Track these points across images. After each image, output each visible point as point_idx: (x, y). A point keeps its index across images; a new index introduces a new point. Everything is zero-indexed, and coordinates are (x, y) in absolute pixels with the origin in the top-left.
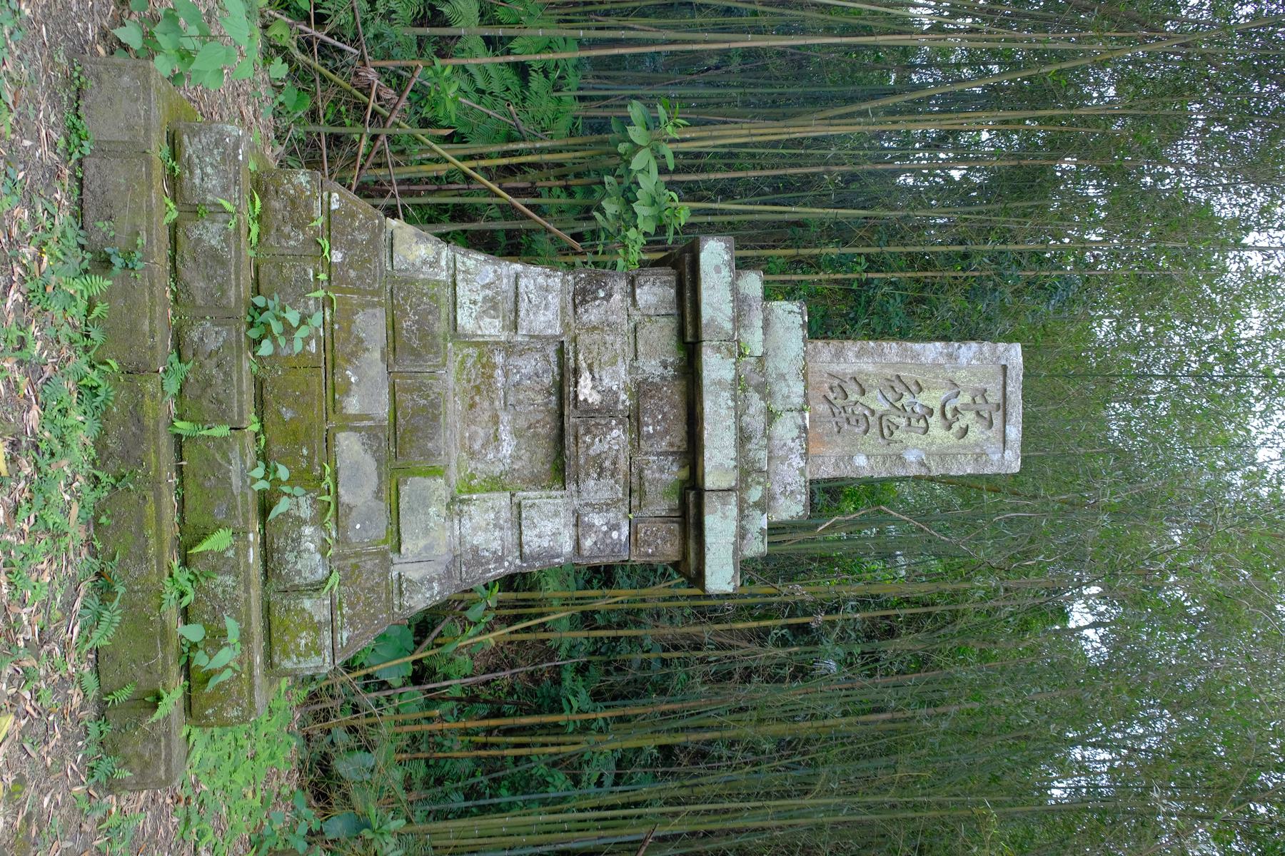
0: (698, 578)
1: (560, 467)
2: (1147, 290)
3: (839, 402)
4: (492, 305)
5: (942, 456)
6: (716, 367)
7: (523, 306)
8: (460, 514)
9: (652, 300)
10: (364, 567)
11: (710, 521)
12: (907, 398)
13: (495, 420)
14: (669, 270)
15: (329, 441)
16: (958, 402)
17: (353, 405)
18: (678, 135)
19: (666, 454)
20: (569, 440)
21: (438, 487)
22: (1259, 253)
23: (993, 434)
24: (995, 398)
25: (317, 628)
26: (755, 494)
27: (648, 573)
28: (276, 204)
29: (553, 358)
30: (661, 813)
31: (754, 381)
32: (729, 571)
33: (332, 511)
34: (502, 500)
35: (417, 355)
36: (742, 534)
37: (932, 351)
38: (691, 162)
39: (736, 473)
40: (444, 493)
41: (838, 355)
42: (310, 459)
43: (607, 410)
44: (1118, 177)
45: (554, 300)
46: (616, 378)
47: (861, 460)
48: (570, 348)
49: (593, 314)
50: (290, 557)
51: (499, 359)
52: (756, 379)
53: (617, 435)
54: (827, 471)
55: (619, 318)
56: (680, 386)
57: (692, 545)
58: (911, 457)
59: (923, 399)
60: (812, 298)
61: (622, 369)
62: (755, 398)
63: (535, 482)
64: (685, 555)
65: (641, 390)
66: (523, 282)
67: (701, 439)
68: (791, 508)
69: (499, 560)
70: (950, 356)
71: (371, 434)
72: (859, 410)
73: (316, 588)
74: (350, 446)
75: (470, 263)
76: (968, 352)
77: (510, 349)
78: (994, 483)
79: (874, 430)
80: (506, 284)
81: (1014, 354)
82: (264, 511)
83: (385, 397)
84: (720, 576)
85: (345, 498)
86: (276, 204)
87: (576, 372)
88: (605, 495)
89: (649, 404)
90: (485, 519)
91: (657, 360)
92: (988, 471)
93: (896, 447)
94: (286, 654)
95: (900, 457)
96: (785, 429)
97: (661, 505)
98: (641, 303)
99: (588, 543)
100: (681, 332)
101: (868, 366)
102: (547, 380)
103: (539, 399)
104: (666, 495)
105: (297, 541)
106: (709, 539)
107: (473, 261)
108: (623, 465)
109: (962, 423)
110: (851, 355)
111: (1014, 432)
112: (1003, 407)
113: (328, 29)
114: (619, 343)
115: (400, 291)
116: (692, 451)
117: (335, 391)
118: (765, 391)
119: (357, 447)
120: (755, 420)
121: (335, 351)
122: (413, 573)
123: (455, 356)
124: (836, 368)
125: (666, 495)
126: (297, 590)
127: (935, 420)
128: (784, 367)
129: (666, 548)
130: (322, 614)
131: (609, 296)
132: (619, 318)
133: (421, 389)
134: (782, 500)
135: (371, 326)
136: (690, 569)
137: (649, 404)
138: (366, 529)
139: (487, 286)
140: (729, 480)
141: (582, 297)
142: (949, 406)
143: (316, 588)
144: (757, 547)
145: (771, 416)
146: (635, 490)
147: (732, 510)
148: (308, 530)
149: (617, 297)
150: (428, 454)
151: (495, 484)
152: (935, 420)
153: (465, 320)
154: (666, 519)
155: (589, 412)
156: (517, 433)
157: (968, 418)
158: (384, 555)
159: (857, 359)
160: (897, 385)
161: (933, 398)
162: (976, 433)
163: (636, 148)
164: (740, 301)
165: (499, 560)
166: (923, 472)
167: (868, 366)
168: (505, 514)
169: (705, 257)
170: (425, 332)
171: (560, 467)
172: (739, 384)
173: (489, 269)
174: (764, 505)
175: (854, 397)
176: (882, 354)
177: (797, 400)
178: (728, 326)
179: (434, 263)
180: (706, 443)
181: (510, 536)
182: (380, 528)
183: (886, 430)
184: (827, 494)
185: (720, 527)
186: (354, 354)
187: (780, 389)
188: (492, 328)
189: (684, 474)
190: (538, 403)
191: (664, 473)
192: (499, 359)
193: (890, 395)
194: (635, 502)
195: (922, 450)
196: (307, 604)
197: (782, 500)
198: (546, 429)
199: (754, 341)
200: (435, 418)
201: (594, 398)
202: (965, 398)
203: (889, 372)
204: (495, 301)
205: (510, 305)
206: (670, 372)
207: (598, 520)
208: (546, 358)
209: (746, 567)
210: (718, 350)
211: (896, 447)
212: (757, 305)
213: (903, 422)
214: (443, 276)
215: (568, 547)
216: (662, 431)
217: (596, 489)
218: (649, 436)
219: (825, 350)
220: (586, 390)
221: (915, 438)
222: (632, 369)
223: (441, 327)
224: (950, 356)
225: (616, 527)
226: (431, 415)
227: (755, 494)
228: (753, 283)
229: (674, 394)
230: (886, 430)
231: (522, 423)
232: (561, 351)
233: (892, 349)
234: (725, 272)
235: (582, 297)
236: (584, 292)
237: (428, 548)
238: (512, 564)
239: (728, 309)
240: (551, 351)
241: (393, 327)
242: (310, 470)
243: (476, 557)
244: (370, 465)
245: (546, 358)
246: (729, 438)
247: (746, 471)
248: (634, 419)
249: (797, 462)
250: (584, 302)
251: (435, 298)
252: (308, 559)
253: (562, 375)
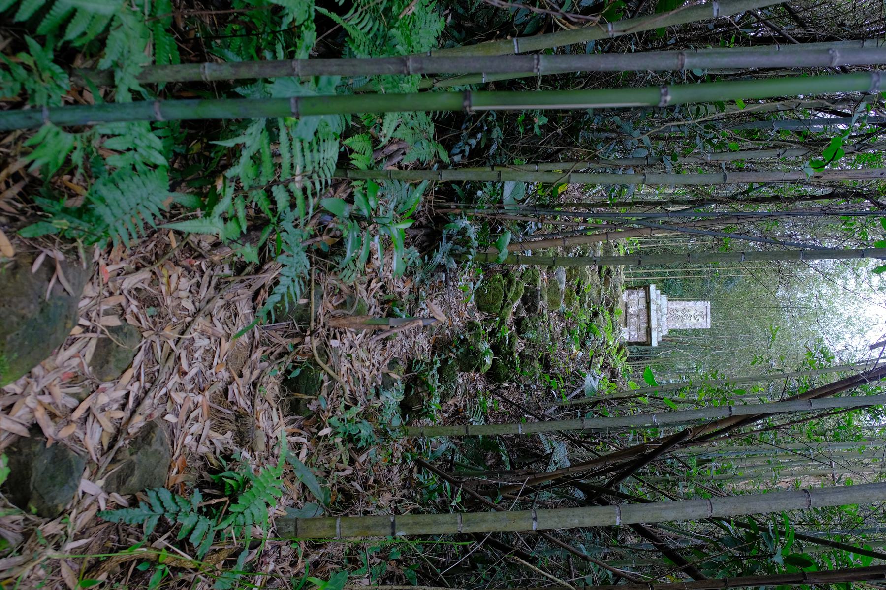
0: (650, 344)
6: (653, 307)
27: (643, 344)
30: (407, 587)
31: (659, 310)
37: (691, 303)
43: (634, 314)
46: (635, 309)
49: (632, 298)
54: (671, 328)
65: (640, 311)
68: (666, 333)
76: (699, 303)
81: (708, 304)
84: (654, 343)
91: (643, 306)
96: (664, 318)
97: (643, 331)
101: (678, 306)
112: (707, 315)
114: (636, 303)
129: (643, 339)
146: (639, 328)
157: (699, 317)
159: (676, 305)
160: (684, 310)
161: (692, 313)
162: (701, 320)
164: (657, 295)
167: (678, 306)
183: (682, 320)
184: (672, 331)
185: (654, 334)
191: (644, 326)
195: (690, 324)
199: (659, 302)
209: (659, 342)
216: (643, 318)
217: (632, 328)
220: (630, 311)
221: (688, 321)
228: (659, 292)
229: (645, 311)
230: (682, 320)
247: (659, 325)
248: (639, 316)
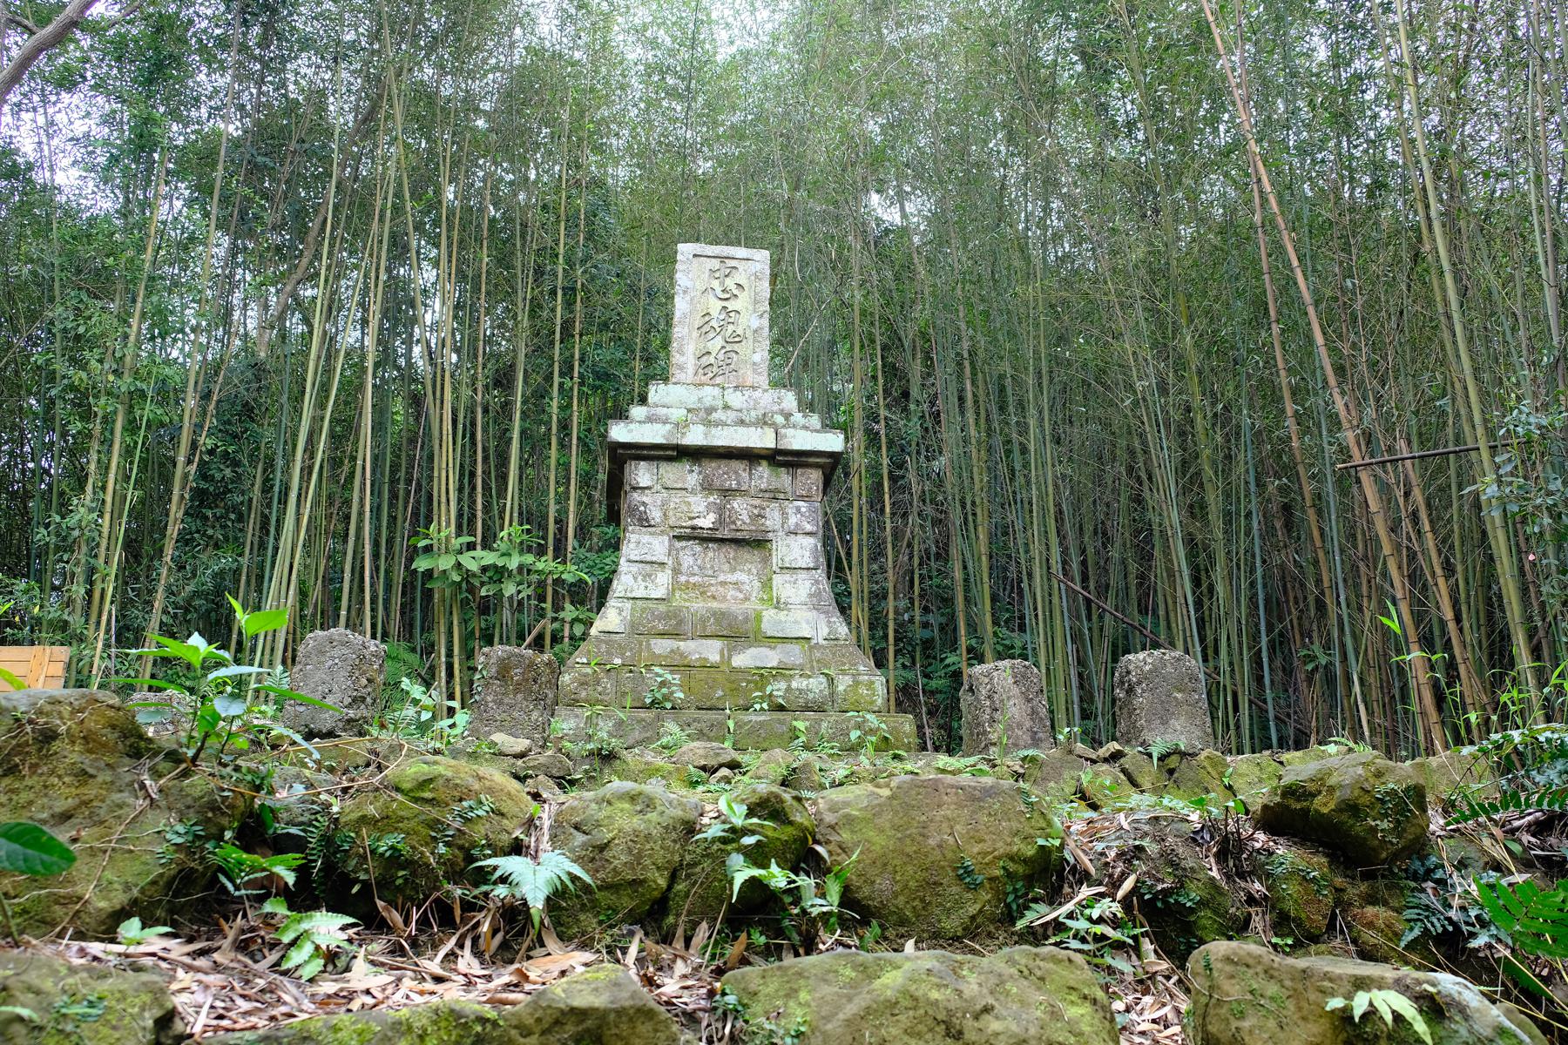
1: (757, 543)
2: (583, 136)
3: (715, 369)
4: (647, 576)
5: (756, 302)
6: (695, 436)
7: (649, 558)
8: (786, 604)
9: (647, 476)
10: (816, 655)
11: (796, 446)
12: (714, 323)
13: (723, 584)
14: (627, 466)
15: (734, 670)
16: (719, 290)
17: (714, 658)
18: (443, 529)
19: (750, 474)
20: (739, 535)
21: (769, 615)
22: (547, 28)
23: (741, 266)
24: (716, 264)
25: (857, 683)
26: (780, 419)
28: (584, 694)
29: (684, 543)
32: (830, 436)
33: (781, 672)
34: (777, 580)
35: (680, 623)
36: (805, 428)
37: (681, 305)
38: (465, 523)
39: (766, 428)
40: (772, 612)
41: (681, 368)
42: (749, 682)
43: (720, 510)
44: (471, 149)
45: (646, 539)
47: (757, 358)
48: (677, 532)
49: (655, 515)
50: (811, 696)
51: (683, 579)
52: (702, 414)
53: (738, 504)
55: (659, 498)
56: (705, 462)
57: (811, 460)
58: (755, 323)
59: (715, 313)
60: (647, 379)
61: (692, 499)
62: (715, 416)
63: (766, 560)
64: (816, 466)
65: (707, 487)
66: (633, 558)
67: (742, 449)
69: (817, 582)
70: (685, 292)
71: (732, 650)
72: (721, 356)
73: (831, 681)
74: (741, 660)
75: (620, 588)
77: (676, 571)
78: (775, 263)
79: (736, 347)
80: (635, 568)
81: (685, 250)
82: (781, 708)
83: (710, 642)
84: (833, 442)
85: (775, 664)
86: (584, 694)
87: (694, 528)
88: (777, 515)
89: (717, 483)
90: (792, 599)
91: (687, 475)
92: (768, 272)
93: (749, 334)
94: (873, 702)
95: (755, 331)
96: (735, 399)
97: (784, 479)
98: (648, 484)
99: (809, 528)
100: (670, 459)
102: (698, 548)
103: (711, 554)
104: (777, 476)
105: (800, 691)
106: (807, 447)
107: (618, 587)
108: (757, 502)
109: (733, 287)
110: (682, 359)
111: (741, 252)
112: (723, 259)
113: (688, 374)
114: (676, 499)
115: (638, 630)
116: (749, 456)
117: (706, 666)
118: (711, 410)
119: (741, 656)
120: (730, 416)
121: (682, 666)
122: (824, 631)
123: (678, 600)
124: (691, 370)
125: (777, 476)
126: (832, 694)
127: (731, 305)
128: (694, 398)
130: (848, 680)
131: (644, 504)
132: (659, 498)
133: (703, 620)
134: (784, 405)
135: (662, 646)
136: (831, 466)
137: (717, 483)
138: (795, 655)
139: (635, 579)
140: (770, 433)
141: (644, 522)
142: (718, 297)
143: (831, 681)
144: (815, 420)
145: (726, 407)
146: (774, 495)
147: (790, 432)
148: (794, 685)
149: (644, 499)
150: (746, 620)
151: (767, 585)
152: (731, 305)
153: (660, 593)
154: (794, 477)
155: (721, 521)
156: (733, 570)
157: (730, 283)
158: (811, 648)
161: (715, 306)
162: (740, 277)
163: (459, 565)
164: (650, 420)
165: (817, 582)
166: (767, 316)
168: (787, 577)
169: (622, 439)
170: (666, 616)
171: (757, 543)
172: (708, 423)
173: (623, 578)
174: (787, 416)
175: (712, 360)
176: (682, 338)
177: (717, 391)
178: (668, 427)
179: (621, 610)
180: (745, 445)
181: (803, 575)
182: (795, 649)
183: (737, 339)
186: (681, 655)
187: (708, 402)
188: (664, 578)
189: (764, 463)
190: (713, 554)
191: (764, 475)
192: (683, 579)
193: (712, 335)
194: (782, 496)
195: (752, 316)
196: (841, 688)
197: (784, 405)
198: (731, 551)
199: (678, 414)
200: (723, 614)
201: (712, 517)
202: (715, 284)
203: (695, 334)
204: (645, 568)
205: (648, 567)
206: (696, 468)
207: (793, 520)
208: (683, 548)
210: (684, 434)
211: (749, 334)
212: (653, 411)
213: (731, 328)
214: (628, 605)
215: (811, 541)
216: (736, 474)
217: (773, 519)
218: (739, 483)
219: (678, 375)
220: (707, 522)
222: (693, 492)
223: (662, 608)
224: (685, 292)
225: (798, 510)
226: (720, 616)
227: (780, 419)
228: (637, 411)
229: (711, 467)
230: (737, 339)
231: (726, 567)
232: (679, 538)
233: (678, 331)
234: (632, 426)
235: (644, 522)
236: (640, 520)
237: (808, 622)
238: (820, 575)
239: (658, 426)
240: (678, 544)
241: (662, 634)
242: (756, 683)
243: (817, 595)
244: (753, 651)
245: (683, 548)
246: (742, 430)
247: (763, 421)
248: (726, 493)
249: (758, 394)
250: (647, 520)
251: (643, 610)
252: (815, 686)
253: (695, 538)
